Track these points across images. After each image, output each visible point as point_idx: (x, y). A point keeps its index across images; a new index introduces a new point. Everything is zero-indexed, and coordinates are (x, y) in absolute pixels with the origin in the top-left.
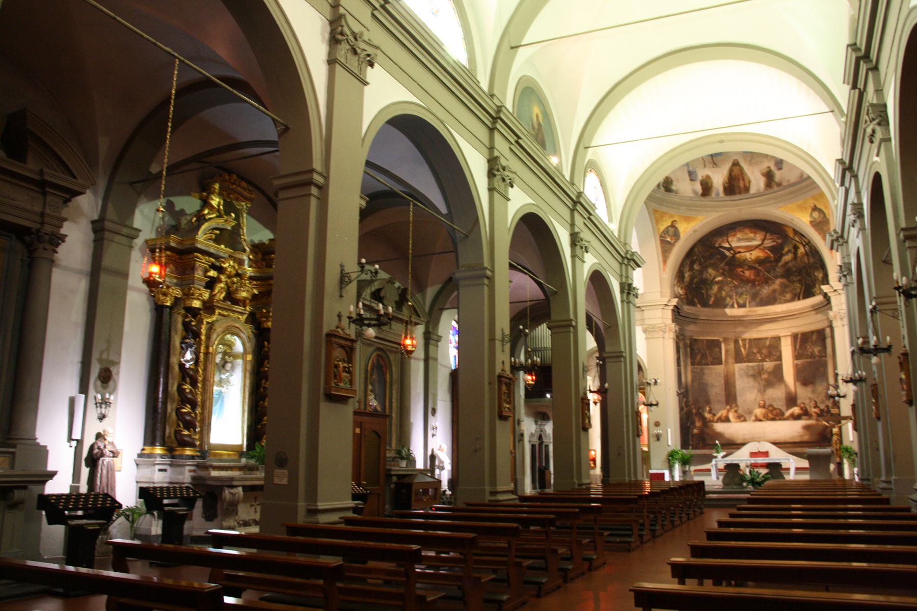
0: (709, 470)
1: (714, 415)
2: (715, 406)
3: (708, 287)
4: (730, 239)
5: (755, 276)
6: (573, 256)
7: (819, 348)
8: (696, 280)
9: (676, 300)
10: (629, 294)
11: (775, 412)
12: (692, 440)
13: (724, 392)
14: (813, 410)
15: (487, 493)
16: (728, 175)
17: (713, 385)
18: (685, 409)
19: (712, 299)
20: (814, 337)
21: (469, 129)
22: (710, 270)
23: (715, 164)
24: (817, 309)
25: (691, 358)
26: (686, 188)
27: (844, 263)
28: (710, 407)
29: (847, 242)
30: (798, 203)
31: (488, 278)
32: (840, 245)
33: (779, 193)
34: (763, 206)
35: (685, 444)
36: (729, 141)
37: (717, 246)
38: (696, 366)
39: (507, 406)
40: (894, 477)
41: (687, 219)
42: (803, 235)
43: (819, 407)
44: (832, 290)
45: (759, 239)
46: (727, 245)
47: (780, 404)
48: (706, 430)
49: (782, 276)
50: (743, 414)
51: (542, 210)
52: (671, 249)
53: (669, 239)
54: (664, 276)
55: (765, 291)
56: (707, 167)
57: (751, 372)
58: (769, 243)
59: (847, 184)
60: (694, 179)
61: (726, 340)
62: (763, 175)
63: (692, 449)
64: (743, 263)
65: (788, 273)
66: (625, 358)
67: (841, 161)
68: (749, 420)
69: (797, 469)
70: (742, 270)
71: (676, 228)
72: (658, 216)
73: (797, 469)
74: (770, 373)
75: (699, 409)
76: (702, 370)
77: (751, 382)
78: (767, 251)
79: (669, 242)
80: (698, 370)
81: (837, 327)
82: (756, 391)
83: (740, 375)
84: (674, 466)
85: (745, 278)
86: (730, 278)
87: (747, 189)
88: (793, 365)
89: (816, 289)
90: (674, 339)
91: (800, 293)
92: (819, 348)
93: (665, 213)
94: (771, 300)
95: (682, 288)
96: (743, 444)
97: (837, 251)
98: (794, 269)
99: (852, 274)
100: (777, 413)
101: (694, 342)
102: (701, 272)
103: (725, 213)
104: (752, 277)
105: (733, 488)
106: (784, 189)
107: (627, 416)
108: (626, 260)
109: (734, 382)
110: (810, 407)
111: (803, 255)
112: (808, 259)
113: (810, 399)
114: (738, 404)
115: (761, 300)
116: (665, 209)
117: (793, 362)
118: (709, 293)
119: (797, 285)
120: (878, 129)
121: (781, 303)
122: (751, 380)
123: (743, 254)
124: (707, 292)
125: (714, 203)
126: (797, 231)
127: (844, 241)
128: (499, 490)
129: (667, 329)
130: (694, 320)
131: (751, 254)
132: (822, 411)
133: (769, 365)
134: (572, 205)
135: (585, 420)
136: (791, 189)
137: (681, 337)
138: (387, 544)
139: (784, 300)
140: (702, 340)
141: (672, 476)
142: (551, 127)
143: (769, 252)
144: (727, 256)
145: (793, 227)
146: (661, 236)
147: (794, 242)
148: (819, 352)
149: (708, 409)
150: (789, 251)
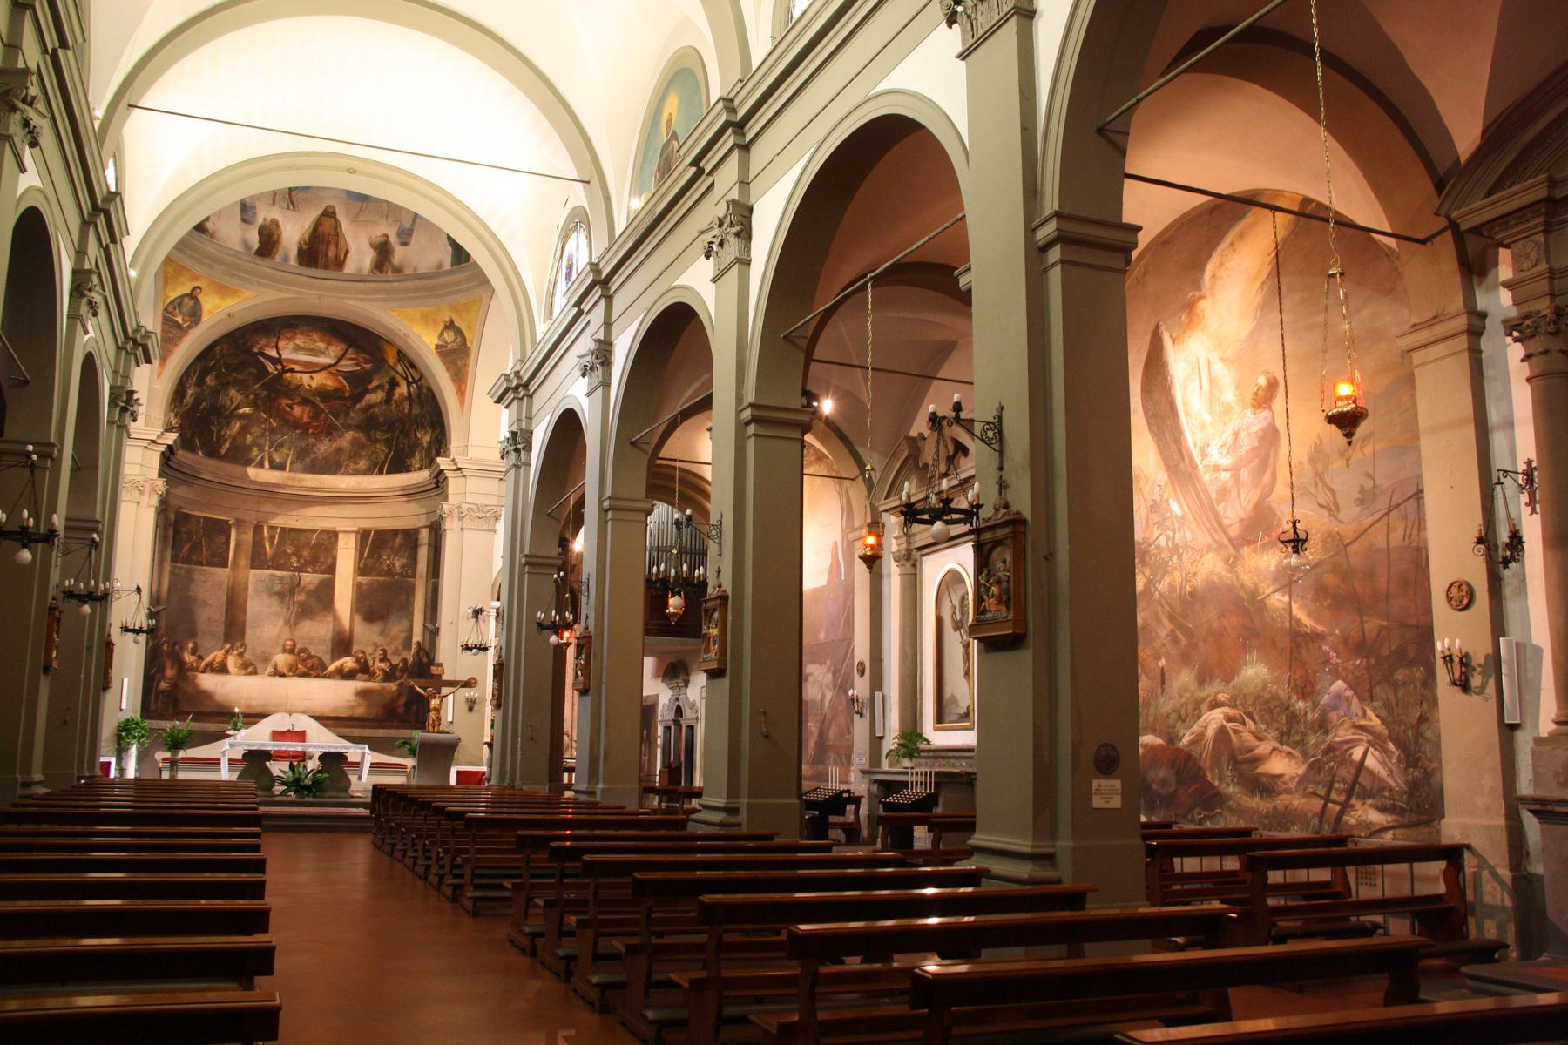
0: (217, 761)
1: (201, 658)
2: (205, 642)
3: (222, 420)
4: (281, 344)
5: (310, 418)
6: (74, 316)
7: (404, 561)
8: (204, 404)
10: (124, 409)
11: (309, 663)
12: (156, 702)
13: (223, 619)
14: (379, 666)
16: (311, 230)
17: (205, 604)
19: (227, 445)
20: (398, 540)
22: (233, 392)
23: (292, 203)
24: (410, 494)
25: (173, 548)
26: (237, 236)
29: (531, 396)
32: (528, 396)
33: (395, 284)
34: (362, 300)
35: (147, 711)
36: (370, 175)
37: (256, 350)
38: (179, 565)
40: (600, 786)
41: (222, 290)
42: (412, 365)
43: (389, 661)
44: (455, 468)
45: (332, 354)
46: (273, 353)
47: (321, 650)
48: (183, 684)
49: (358, 428)
50: (253, 661)
51: (49, 205)
52: (181, 338)
53: (179, 319)
55: (324, 447)
56: (277, 202)
57: (277, 588)
58: (347, 366)
59: (586, 306)
62: (374, 246)
63: (192, 720)
64: (294, 391)
65: (369, 424)
69: (373, 765)
70: (289, 402)
71: (197, 302)
72: (170, 270)
73: (373, 765)
74: (310, 593)
75: (175, 644)
76: (189, 572)
77: (275, 605)
78: (340, 378)
79: (178, 325)
80: (183, 572)
82: (281, 622)
83: (256, 590)
85: (292, 418)
87: (339, 264)
88: (353, 584)
92: (404, 561)
93: (183, 267)
94: (331, 466)
95: (176, 416)
96: (266, 716)
97: (506, 407)
98: (382, 419)
100: (314, 663)
101: (183, 518)
102: (216, 392)
103: (292, 296)
107: (89, 648)
108: (131, 343)
109: (245, 601)
110: (374, 659)
111: (404, 399)
112: (411, 408)
113: (376, 646)
114: (247, 642)
115: (314, 461)
118: (223, 433)
119: (382, 447)
120: (732, 239)
122: (275, 602)
123: (299, 375)
124: (220, 431)
125: (278, 273)
126: (404, 355)
129: (148, 489)
131: (312, 378)
132: (393, 667)
133: (310, 578)
134: (89, 213)
135: (51, 653)
136: (419, 283)
140: (200, 517)
141: (121, 770)
144: (269, 373)
145: (401, 345)
146: (165, 309)
147: (393, 373)
148: (403, 567)
149: (190, 645)
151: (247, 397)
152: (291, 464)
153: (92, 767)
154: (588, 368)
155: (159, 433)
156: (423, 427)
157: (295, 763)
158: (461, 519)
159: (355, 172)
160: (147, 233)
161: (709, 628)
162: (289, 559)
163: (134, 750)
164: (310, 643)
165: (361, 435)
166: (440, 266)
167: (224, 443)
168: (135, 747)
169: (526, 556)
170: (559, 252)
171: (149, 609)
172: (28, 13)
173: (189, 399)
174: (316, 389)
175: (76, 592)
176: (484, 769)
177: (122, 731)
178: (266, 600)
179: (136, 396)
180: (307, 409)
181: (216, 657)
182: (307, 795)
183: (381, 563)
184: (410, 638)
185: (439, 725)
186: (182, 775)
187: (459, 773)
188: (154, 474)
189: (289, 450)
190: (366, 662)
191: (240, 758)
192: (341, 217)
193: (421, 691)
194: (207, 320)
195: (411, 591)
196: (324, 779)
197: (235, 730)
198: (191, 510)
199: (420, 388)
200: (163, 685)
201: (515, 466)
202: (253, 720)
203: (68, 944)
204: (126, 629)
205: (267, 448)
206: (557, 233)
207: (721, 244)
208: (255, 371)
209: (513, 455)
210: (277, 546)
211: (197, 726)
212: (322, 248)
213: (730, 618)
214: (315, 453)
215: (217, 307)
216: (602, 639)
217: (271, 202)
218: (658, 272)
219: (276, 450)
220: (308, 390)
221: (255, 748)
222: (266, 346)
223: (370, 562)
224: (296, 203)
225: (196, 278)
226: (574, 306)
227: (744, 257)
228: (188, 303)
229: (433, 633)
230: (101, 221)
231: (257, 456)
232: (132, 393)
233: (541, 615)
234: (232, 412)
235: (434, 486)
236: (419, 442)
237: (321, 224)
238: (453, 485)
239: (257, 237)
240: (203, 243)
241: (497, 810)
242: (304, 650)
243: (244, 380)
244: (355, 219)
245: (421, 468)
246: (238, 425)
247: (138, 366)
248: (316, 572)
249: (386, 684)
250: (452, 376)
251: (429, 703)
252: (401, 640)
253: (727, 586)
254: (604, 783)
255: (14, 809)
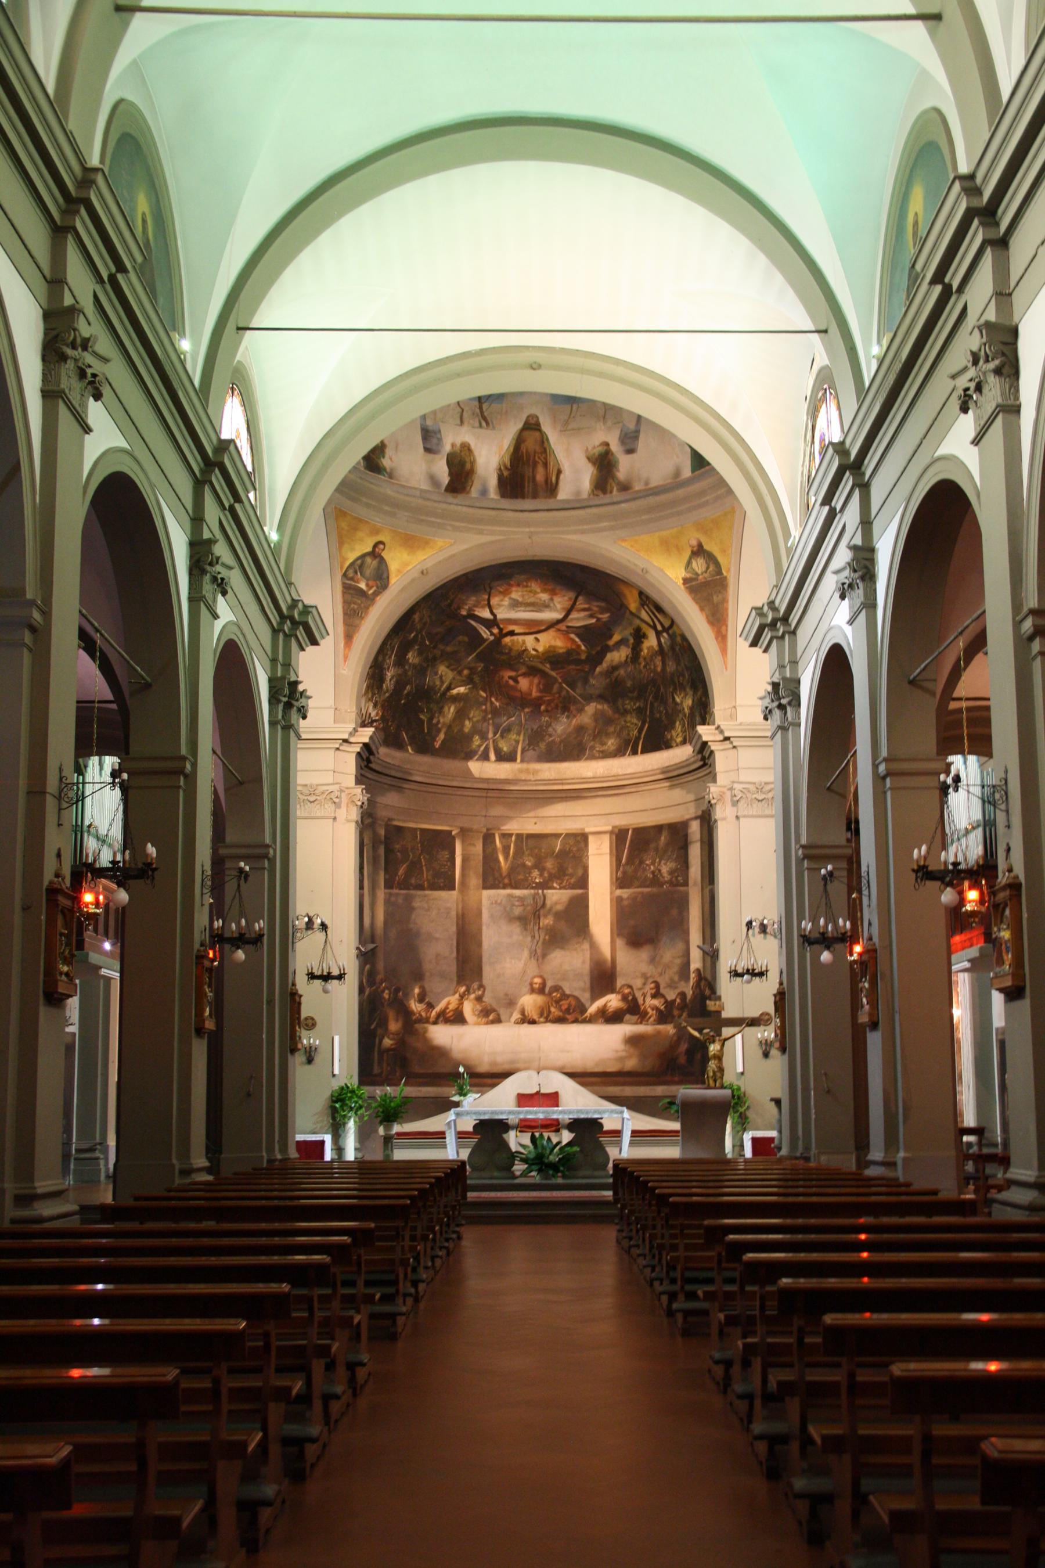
0: (441, 1135)
1: (431, 1006)
2: (434, 985)
4: (494, 601)
5: (541, 691)
7: (672, 865)
8: (408, 688)
9: (370, 731)
10: (288, 706)
11: (565, 1004)
13: (454, 955)
14: (651, 1003)
15: (9, 1200)
16: (512, 449)
18: (367, 992)
19: (442, 736)
20: (663, 839)
21: (11, 216)
22: (442, 669)
24: (673, 776)
25: (386, 870)
27: (784, 679)
28: (422, 988)
29: (794, 633)
30: (665, 533)
31: (33, 629)
32: (777, 638)
33: (623, 505)
34: (583, 532)
35: (367, 1074)
37: (464, 613)
39: (65, 969)
41: (410, 542)
42: (659, 609)
43: (663, 996)
44: (721, 738)
45: (559, 606)
46: (486, 614)
47: (577, 987)
49: (601, 698)
50: (495, 1005)
52: (367, 608)
53: (363, 585)
54: (344, 672)
55: (561, 727)
56: (466, 423)
57: (518, 911)
58: (579, 619)
59: (838, 502)
60: (434, 447)
61: (464, 832)
63: (406, 1084)
64: (517, 659)
66: (272, 861)
67: (840, 449)
68: (509, 1021)
69: (635, 1133)
70: (513, 674)
71: (382, 560)
72: (344, 525)
73: (635, 1133)
74: (558, 915)
75: (397, 990)
76: (408, 899)
78: (573, 636)
79: (362, 593)
80: (400, 901)
81: (724, 819)
83: (492, 916)
84: (345, 1124)
85: (518, 694)
86: (485, 691)
87: (551, 489)
89: (674, 733)
90: (357, 822)
91: (638, 739)
92: (672, 865)
93: (360, 520)
95: (375, 706)
96: (505, 1075)
97: (766, 651)
99: (799, 705)
100: (570, 1005)
101: (396, 832)
102: (421, 671)
104: (535, 694)
105: (492, 1178)
106: (634, 499)
107: (271, 1002)
108: (288, 622)
111: (653, 654)
113: (645, 977)
114: (485, 982)
115: (550, 745)
116: (362, 512)
117: (612, 893)
118: (435, 721)
119: (633, 720)
120: (992, 380)
121: (592, 757)
122: (516, 928)
123: (520, 638)
124: (431, 719)
126: (648, 597)
127: (787, 629)
128: (39, 1191)
129: (344, 797)
130: (398, 781)
131: (537, 640)
132: (669, 1004)
133: (557, 896)
134: (201, 470)
135: (204, 1011)
136: (652, 500)
137: (368, 821)
138: (28, 1372)
139: (602, 752)
140: (415, 830)
141: (339, 1150)
142: (169, 262)
143: (577, 640)
144: (483, 640)
145: (640, 583)
146: (345, 575)
147: (637, 622)
148: (671, 872)
150: (622, 642)
151: (460, 673)
152: (522, 753)
153: (284, 1148)
154: (846, 586)
155: (351, 730)
156: (683, 688)
157: (537, 1135)
158: (735, 803)
159: (540, 367)
160: (295, 483)
161: (999, 930)
162: (530, 873)
163: (351, 1125)
164: (564, 979)
165: (606, 707)
166: (677, 473)
167: (437, 736)
168: (352, 1120)
169: (803, 847)
170: (809, 434)
171: (358, 948)
172: (69, 236)
173: (389, 684)
174: (543, 654)
175: (227, 935)
176: (773, 1134)
177: (336, 1102)
178: (505, 927)
179: (301, 688)
180: (536, 681)
181: (449, 1003)
182: (553, 1176)
183: (645, 870)
184: (687, 964)
185: (722, 1078)
186: (400, 1154)
187: (755, 1141)
188: (351, 781)
189: (519, 734)
190: (635, 999)
191: (471, 1129)
192: (547, 428)
193: (696, 1034)
194: (395, 580)
195: (683, 904)
196: (574, 1153)
197: (461, 1094)
198: (404, 821)
199: (672, 637)
200: (387, 1042)
201: (780, 727)
202: (489, 1081)
203: (49, 1375)
204: (312, 976)
205: (490, 735)
206: (805, 406)
207: (979, 388)
208: (466, 639)
209: (777, 714)
210: (514, 858)
211: (412, 1091)
212: (528, 472)
213: (1025, 915)
214: (550, 736)
215: (407, 565)
216: (891, 953)
217: (459, 422)
218: (918, 441)
219: (502, 736)
220: (534, 656)
221: (486, 1117)
222: (476, 606)
223: (630, 869)
224: (489, 420)
225: (376, 531)
226: (823, 504)
227: (1009, 402)
228: (371, 563)
229: (712, 955)
230: (217, 478)
231: (479, 746)
232: (296, 683)
233: (807, 926)
234: (444, 694)
235: (701, 763)
236: (679, 708)
237: (524, 441)
238: (722, 760)
239: (446, 469)
240: (378, 484)
241: (790, 1190)
242: (557, 988)
243: (455, 653)
244: (566, 428)
245: (684, 742)
246: (452, 709)
247: (303, 649)
248: (564, 888)
249: (661, 1027)
250: (707, 617)
251: (707, 1049)
252: (676, 969)
253: (1019, 870)
254: (906, 1150)
255: (139, 1203)
